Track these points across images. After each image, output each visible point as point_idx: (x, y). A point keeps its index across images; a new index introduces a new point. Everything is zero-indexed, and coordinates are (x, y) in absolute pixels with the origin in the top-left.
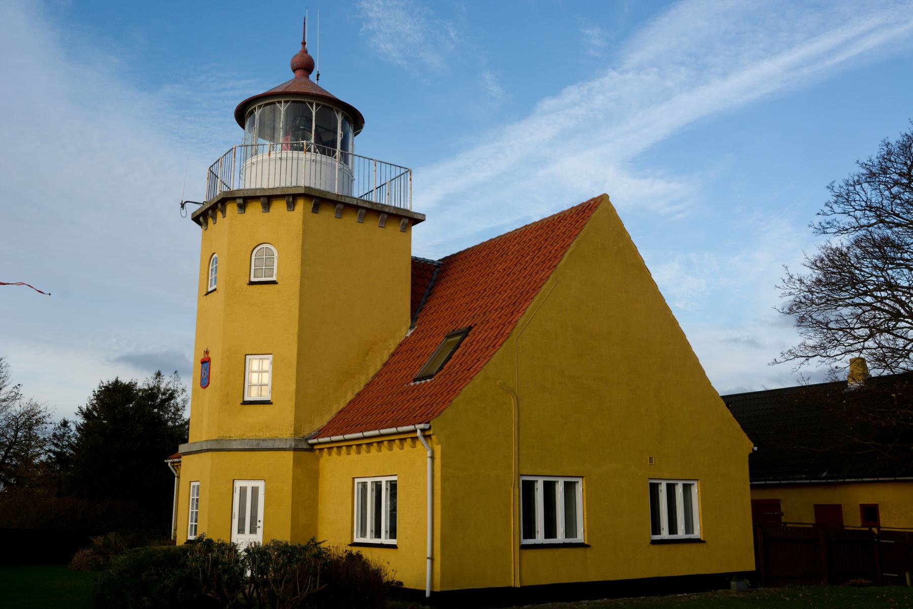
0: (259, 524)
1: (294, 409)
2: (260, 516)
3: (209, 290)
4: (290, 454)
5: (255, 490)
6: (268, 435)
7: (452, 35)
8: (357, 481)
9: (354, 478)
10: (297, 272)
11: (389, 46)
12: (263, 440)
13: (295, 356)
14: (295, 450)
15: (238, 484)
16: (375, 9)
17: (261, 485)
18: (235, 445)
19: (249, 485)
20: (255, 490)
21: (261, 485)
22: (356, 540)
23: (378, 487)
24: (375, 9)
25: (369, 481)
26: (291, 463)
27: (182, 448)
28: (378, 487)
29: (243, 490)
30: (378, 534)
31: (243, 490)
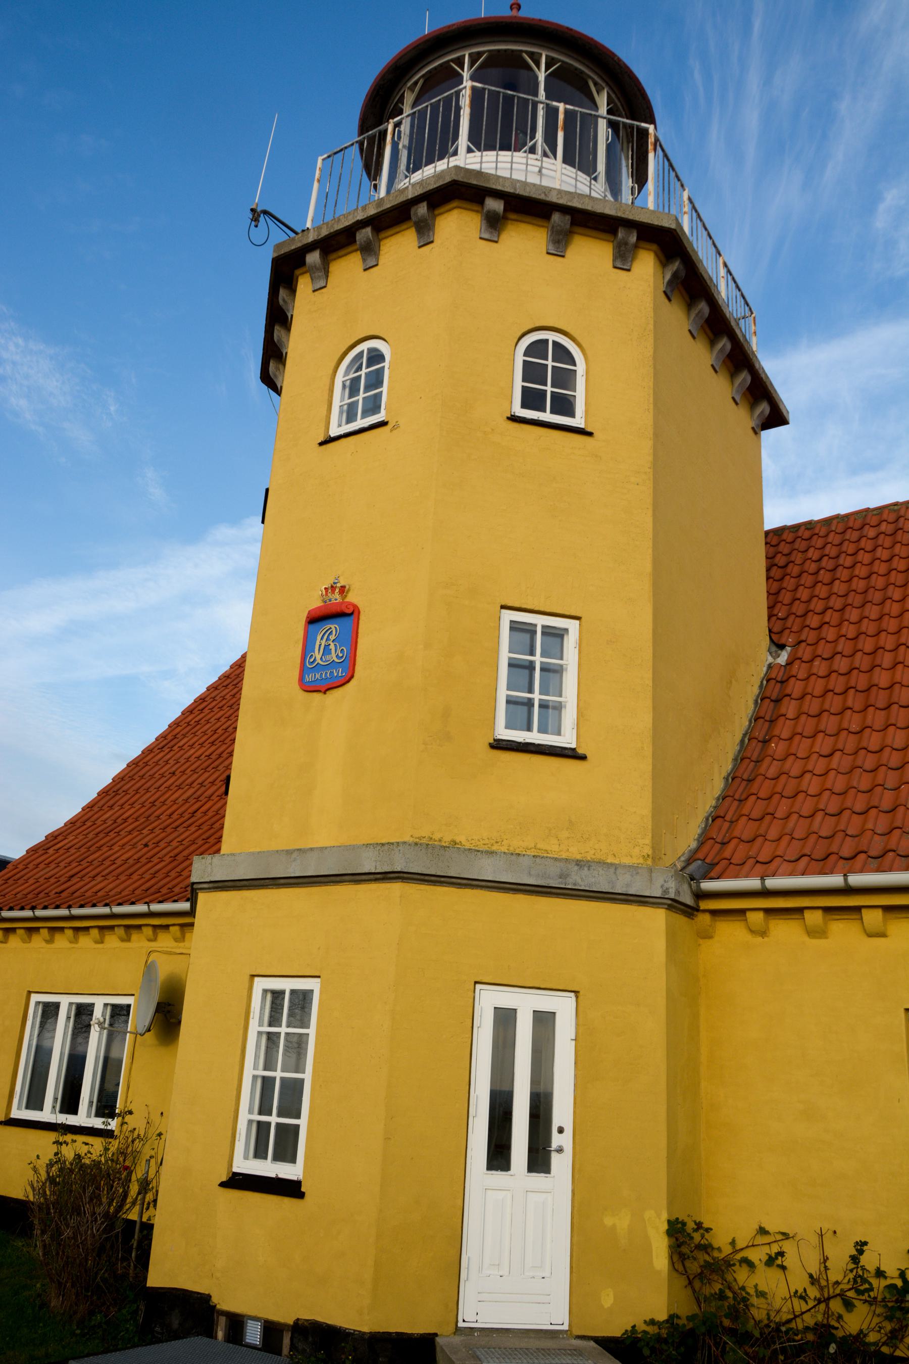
0: (556, 1140)
1: (649, 784)
2: (562, 1112)
3: (334, 432)
4: (658, 917)
5: (544, 1022)
6: (575, 851)
7: (112, 408)
8: (35, 998)
9: (30, 993)
10: (646, 419)
11: (23, 403)
12: (579, 863)
13: (649, 636)
14: (674, 905)
15: (490, 1000)
16: (12, 348)
17: (563, 1007)
18: (487, 870)
19: (526, 1004)
20: (544, 1022)
21: (563, 1007)
22: (16, 1114)
23: (83, 1012)
24: (12, 348)
25: (65, 1001)
26: (660, 944)
27: (203, 869)
28: (83, 1012)
29: (505, 1019)
30: (70, 1103)
31: (505, 1019)
